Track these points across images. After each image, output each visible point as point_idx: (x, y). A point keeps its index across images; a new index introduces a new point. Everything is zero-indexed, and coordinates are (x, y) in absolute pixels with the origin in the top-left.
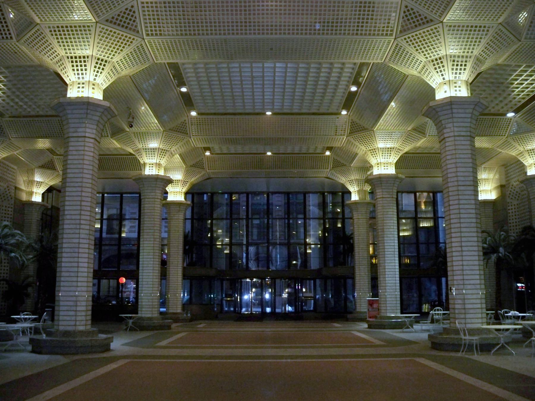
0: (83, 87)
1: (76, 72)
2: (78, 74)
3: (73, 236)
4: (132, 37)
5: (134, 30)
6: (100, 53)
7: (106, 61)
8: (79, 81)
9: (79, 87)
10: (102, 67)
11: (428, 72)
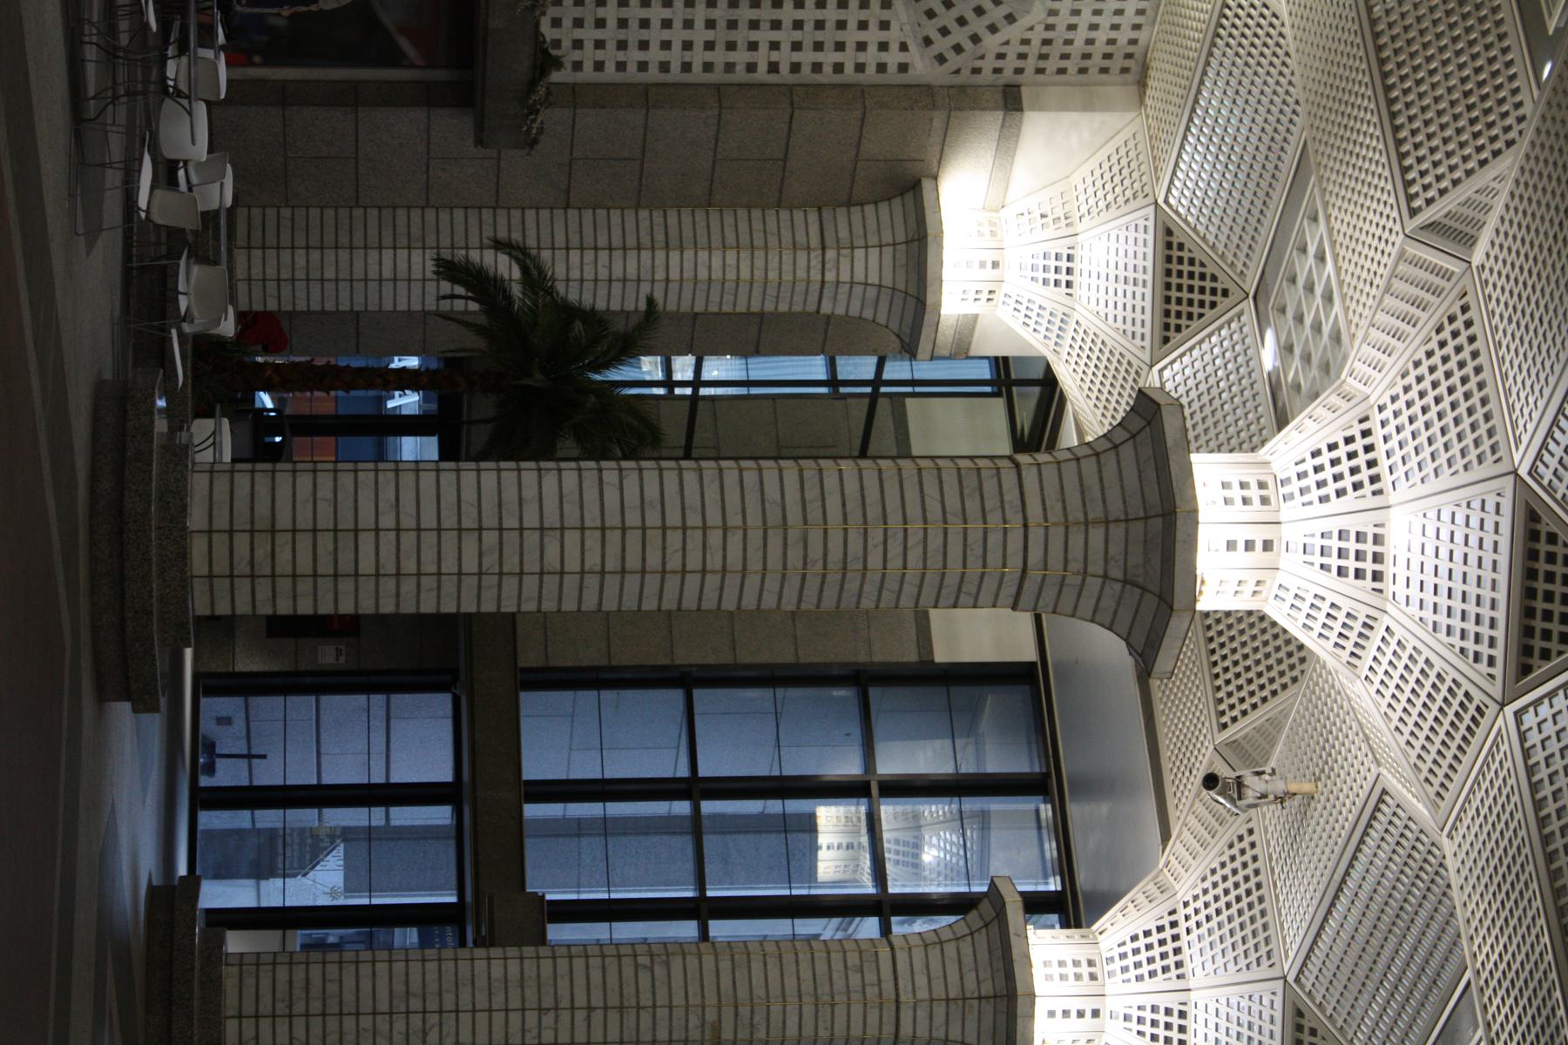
1: (1309, 465)
2: (1123, 956)
4: (1498, 653)
5: (1527, 651)
9: (1243, 485)
10: (1351, 564)
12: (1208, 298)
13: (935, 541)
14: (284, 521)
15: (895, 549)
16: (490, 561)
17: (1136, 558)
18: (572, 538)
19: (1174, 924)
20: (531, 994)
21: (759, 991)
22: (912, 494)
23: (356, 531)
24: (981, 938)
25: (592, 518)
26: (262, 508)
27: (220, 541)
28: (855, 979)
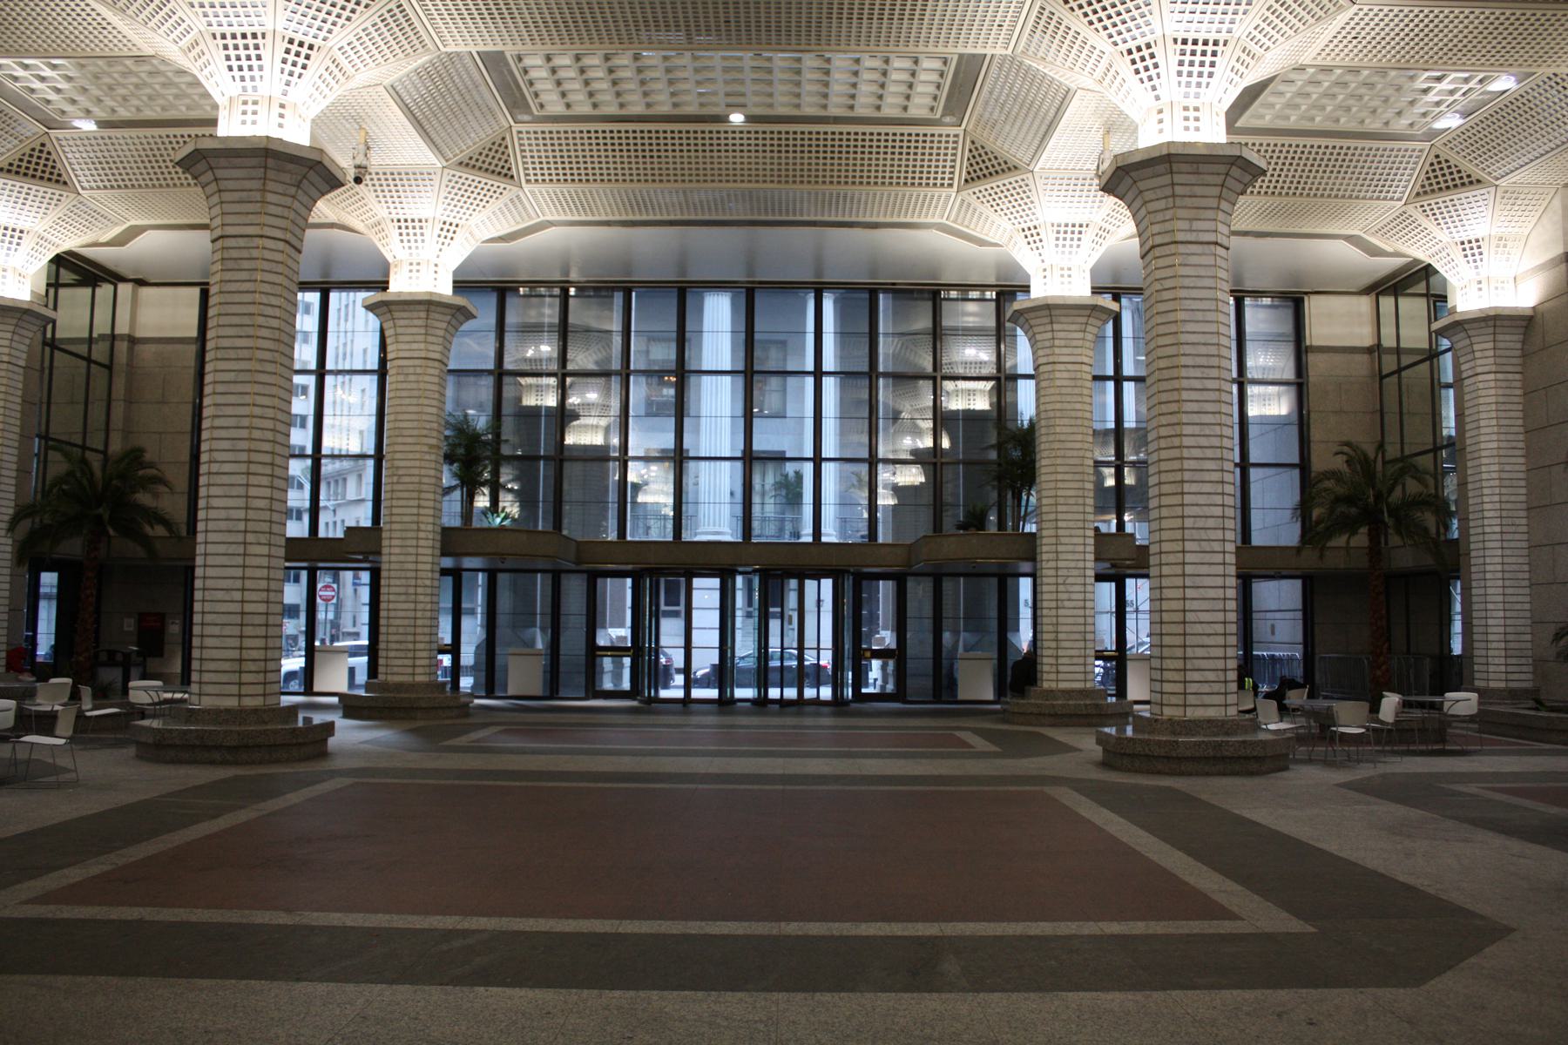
0: (255, 113)
3: (1514, 599)
6: (294, 25)
7: (1216, 43)
8: (1186, 103)
9: (244, 113)
10: (1149, 62)
11: (1119, 79)
12: (44, 155)
13: (267, 288)
14: (235, 654)
15: (269, 311)
16: (263, 539)
17: (286, 178)
18: (253, 492)
19: (224, 37)
20: (410, 535)
21: (415, 424)
22: (237, 298)
23: (243, 613)
24: (396, 315)
25: (242, 480)
26: (226, 666)
27: (245, 690)
28: (412, 378)
